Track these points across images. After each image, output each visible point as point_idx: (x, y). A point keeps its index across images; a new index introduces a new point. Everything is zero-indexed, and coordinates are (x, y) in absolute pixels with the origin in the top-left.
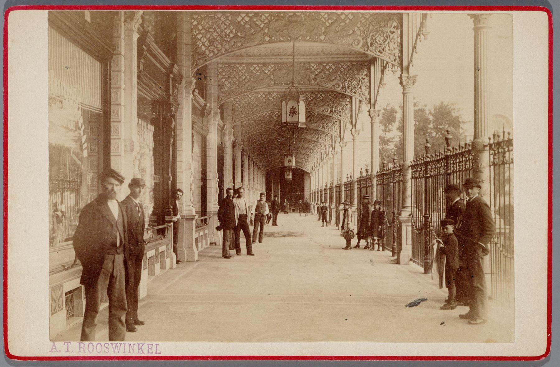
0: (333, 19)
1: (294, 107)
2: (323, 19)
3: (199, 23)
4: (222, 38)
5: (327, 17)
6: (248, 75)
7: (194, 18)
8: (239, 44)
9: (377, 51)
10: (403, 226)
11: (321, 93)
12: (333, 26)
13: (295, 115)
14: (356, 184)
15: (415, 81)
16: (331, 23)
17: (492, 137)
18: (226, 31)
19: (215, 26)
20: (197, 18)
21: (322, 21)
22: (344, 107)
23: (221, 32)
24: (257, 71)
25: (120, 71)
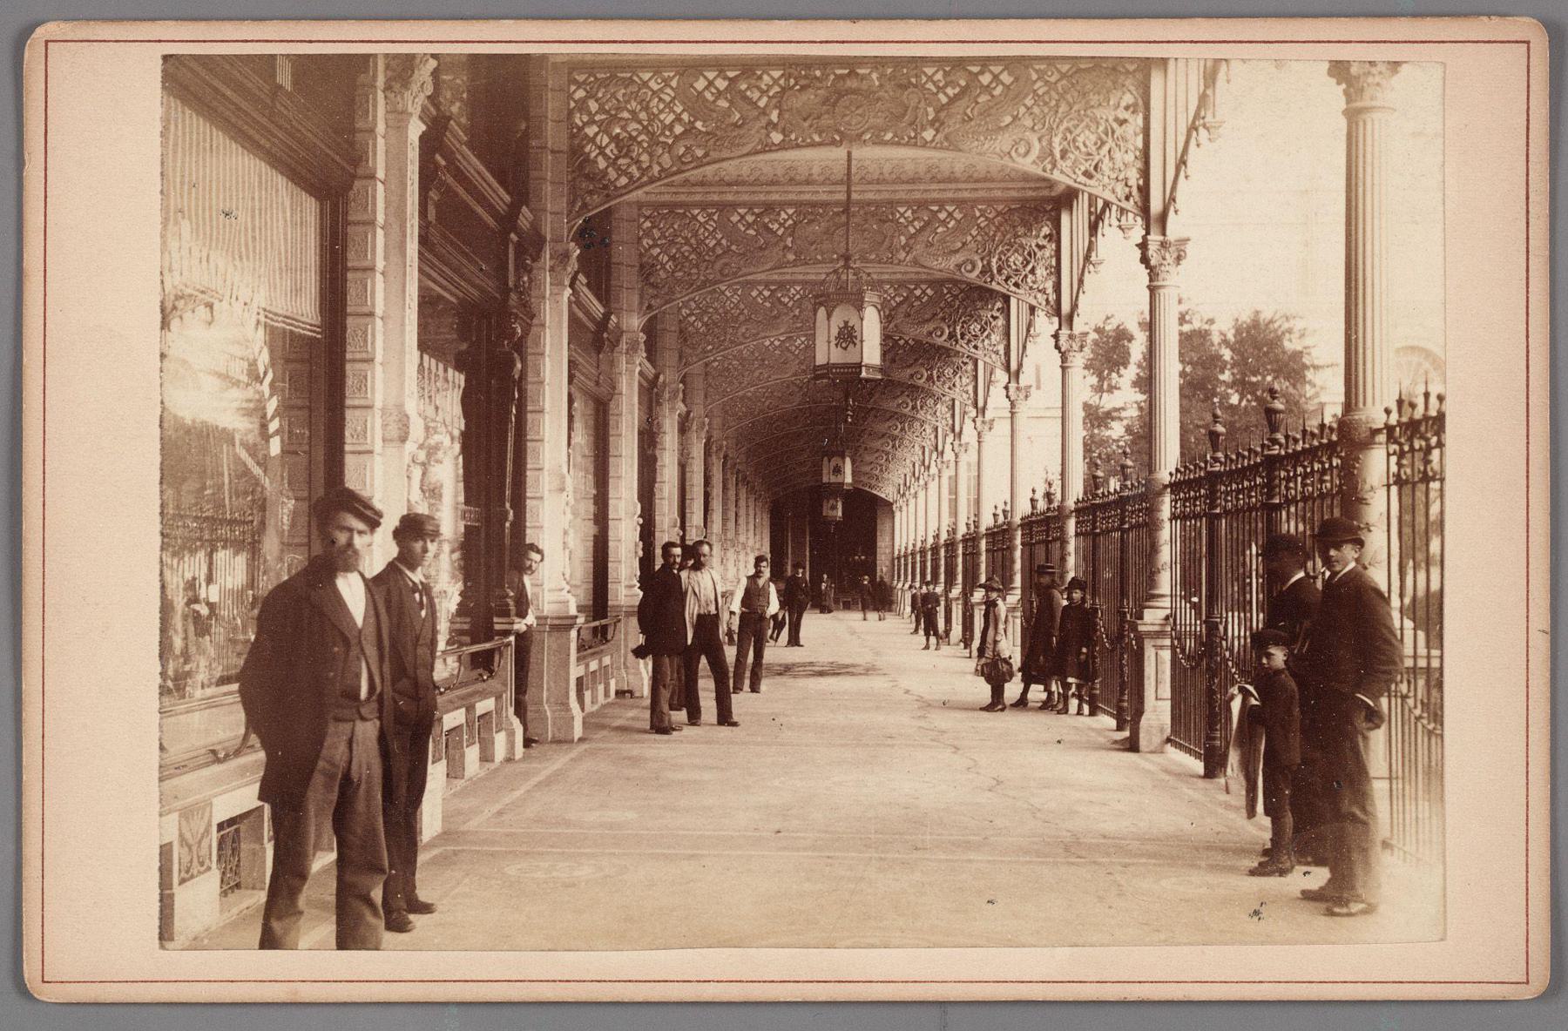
0: (959, 85)
1: (850, 324)
4: (652, 135)
6: (683, 110)
7: (575, 82)
8: (699, 153)
9: (1079, 173)
10: (1149, 653)
11: (950, 209)
13: (851, 345)
15: (1182, 253)
16: (952, 95)
18: (662, 117)
20: (584, 82)
22: (986, 323)
23: (650, 120)
24: (749, 226)
25: (372, 223)
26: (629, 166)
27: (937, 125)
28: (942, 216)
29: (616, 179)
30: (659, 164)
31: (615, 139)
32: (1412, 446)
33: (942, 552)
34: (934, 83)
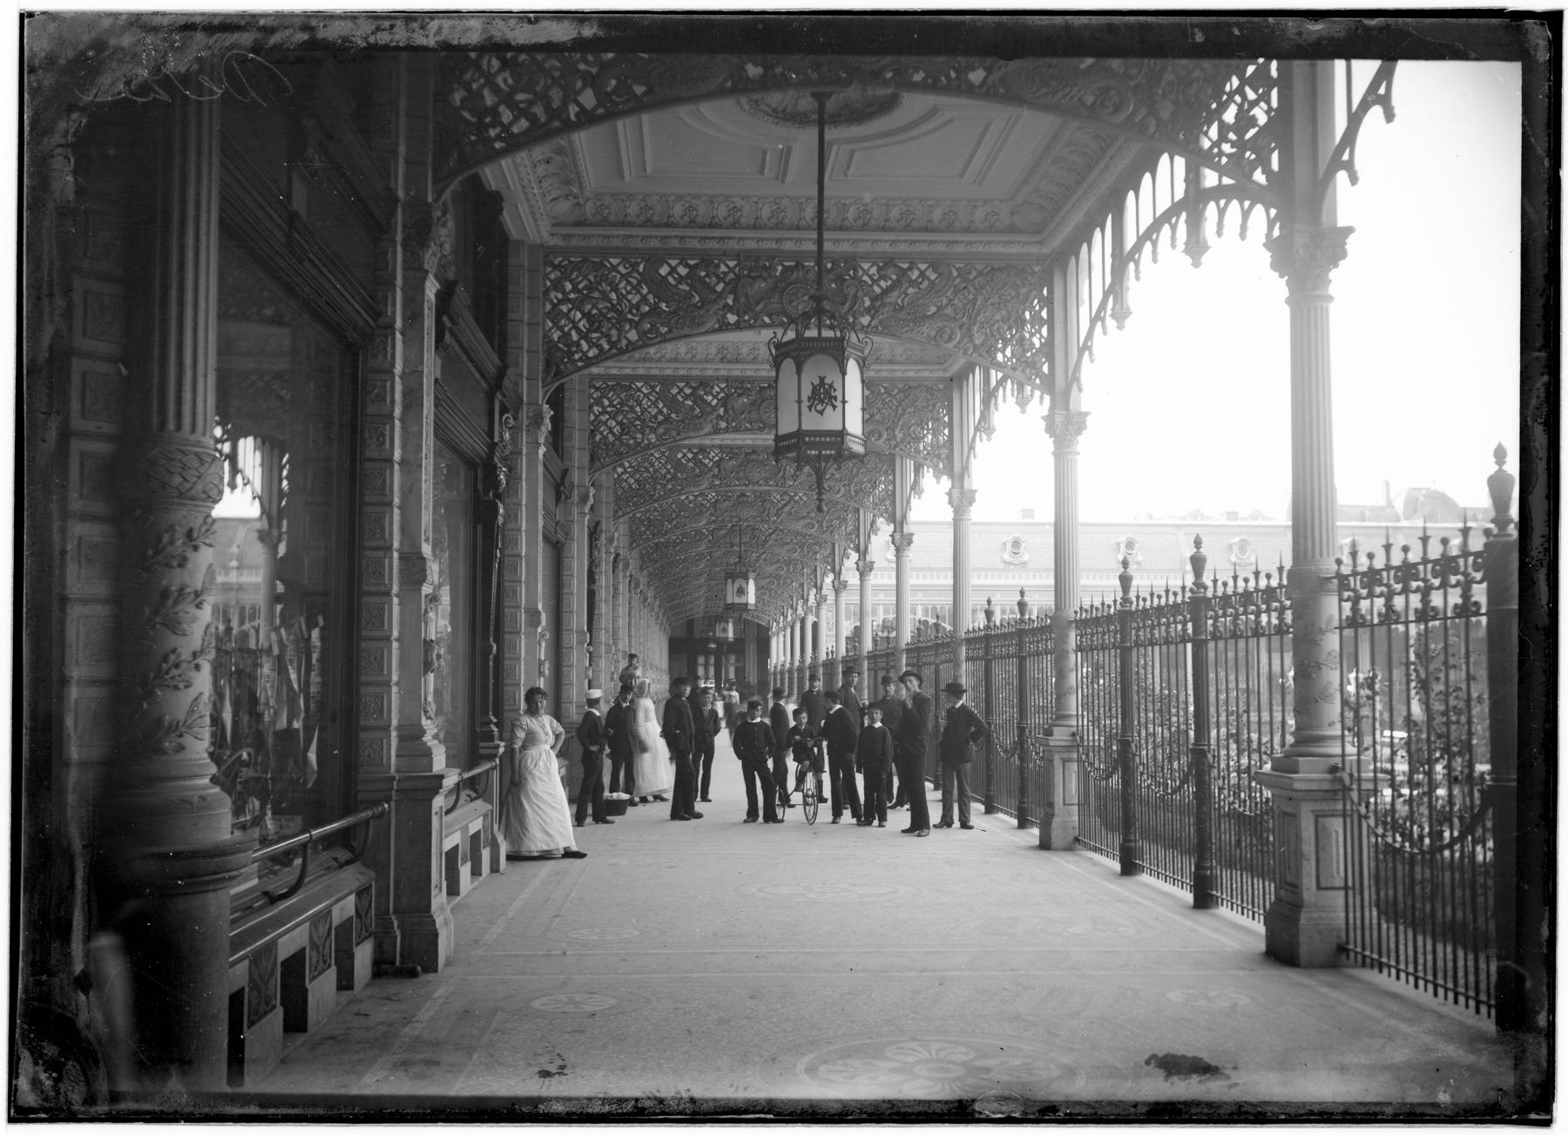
1: (827, 381)
2: (865, 278)
3: (604, 396)
4: (643, 421)
11: (923, 267)
13: (829, 408)
17: (1163, 594)
18: (630, 297)
20: (559, 265)
24: (686, 397)
25: (572, 575)
26: (599, 338)
29: (511, 124)
30: (578, 104)
31: (620, 423)
34: (870, 276)
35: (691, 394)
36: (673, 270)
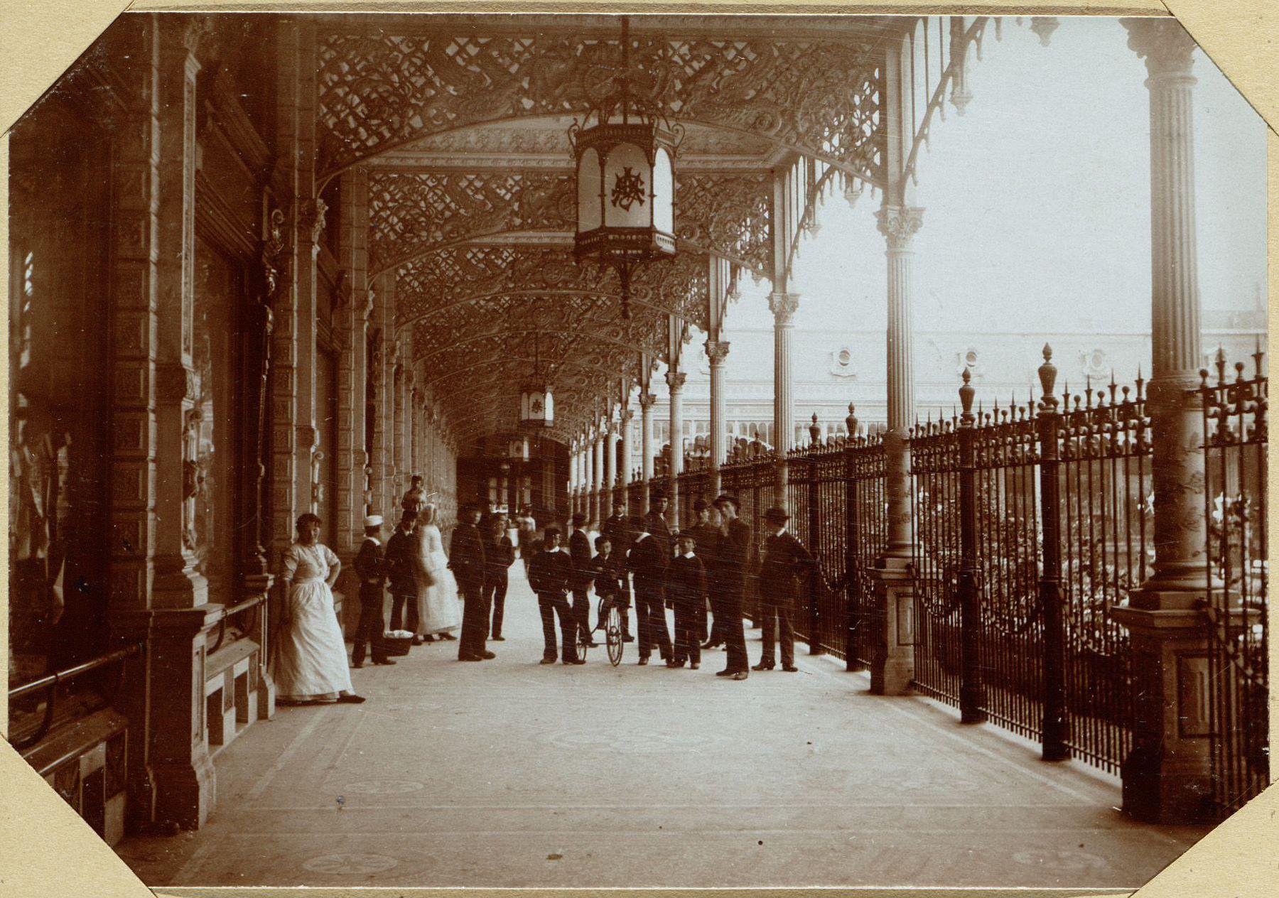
0: (705, 60)
1: (634, 173)
5: (687, 52)
12: (705, 76)
13: (636, 203)
14: (677, 486)
16: (697, 68)
19: (415, 196)
21: (676, 63)
23: (427, 207)
24: (477, 191)
26: (412, 238)
27: (684, 96)
28: (731, 55)
32: (987, 444)
33: (598, 499)
35: (478, 55)
36: (462, 49)
